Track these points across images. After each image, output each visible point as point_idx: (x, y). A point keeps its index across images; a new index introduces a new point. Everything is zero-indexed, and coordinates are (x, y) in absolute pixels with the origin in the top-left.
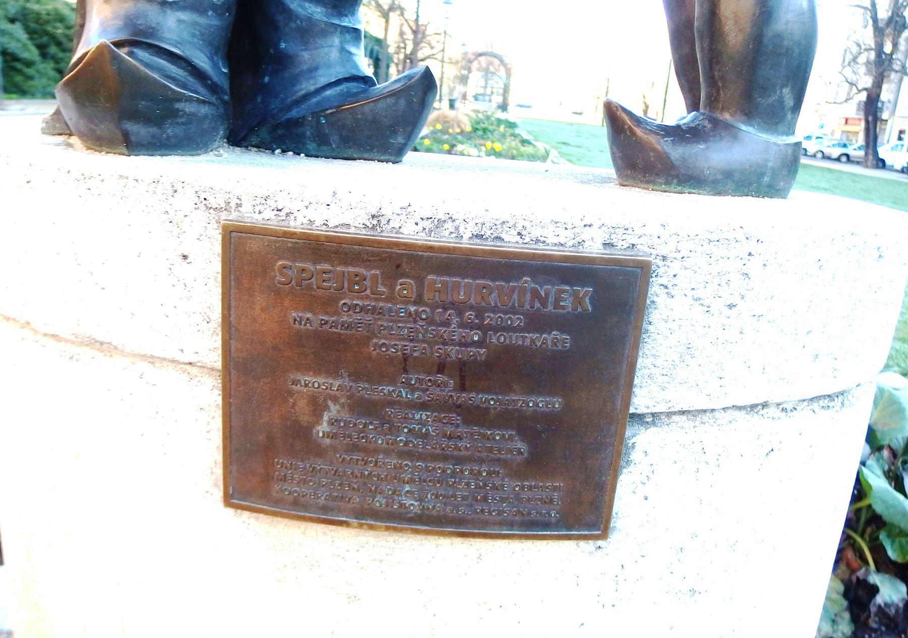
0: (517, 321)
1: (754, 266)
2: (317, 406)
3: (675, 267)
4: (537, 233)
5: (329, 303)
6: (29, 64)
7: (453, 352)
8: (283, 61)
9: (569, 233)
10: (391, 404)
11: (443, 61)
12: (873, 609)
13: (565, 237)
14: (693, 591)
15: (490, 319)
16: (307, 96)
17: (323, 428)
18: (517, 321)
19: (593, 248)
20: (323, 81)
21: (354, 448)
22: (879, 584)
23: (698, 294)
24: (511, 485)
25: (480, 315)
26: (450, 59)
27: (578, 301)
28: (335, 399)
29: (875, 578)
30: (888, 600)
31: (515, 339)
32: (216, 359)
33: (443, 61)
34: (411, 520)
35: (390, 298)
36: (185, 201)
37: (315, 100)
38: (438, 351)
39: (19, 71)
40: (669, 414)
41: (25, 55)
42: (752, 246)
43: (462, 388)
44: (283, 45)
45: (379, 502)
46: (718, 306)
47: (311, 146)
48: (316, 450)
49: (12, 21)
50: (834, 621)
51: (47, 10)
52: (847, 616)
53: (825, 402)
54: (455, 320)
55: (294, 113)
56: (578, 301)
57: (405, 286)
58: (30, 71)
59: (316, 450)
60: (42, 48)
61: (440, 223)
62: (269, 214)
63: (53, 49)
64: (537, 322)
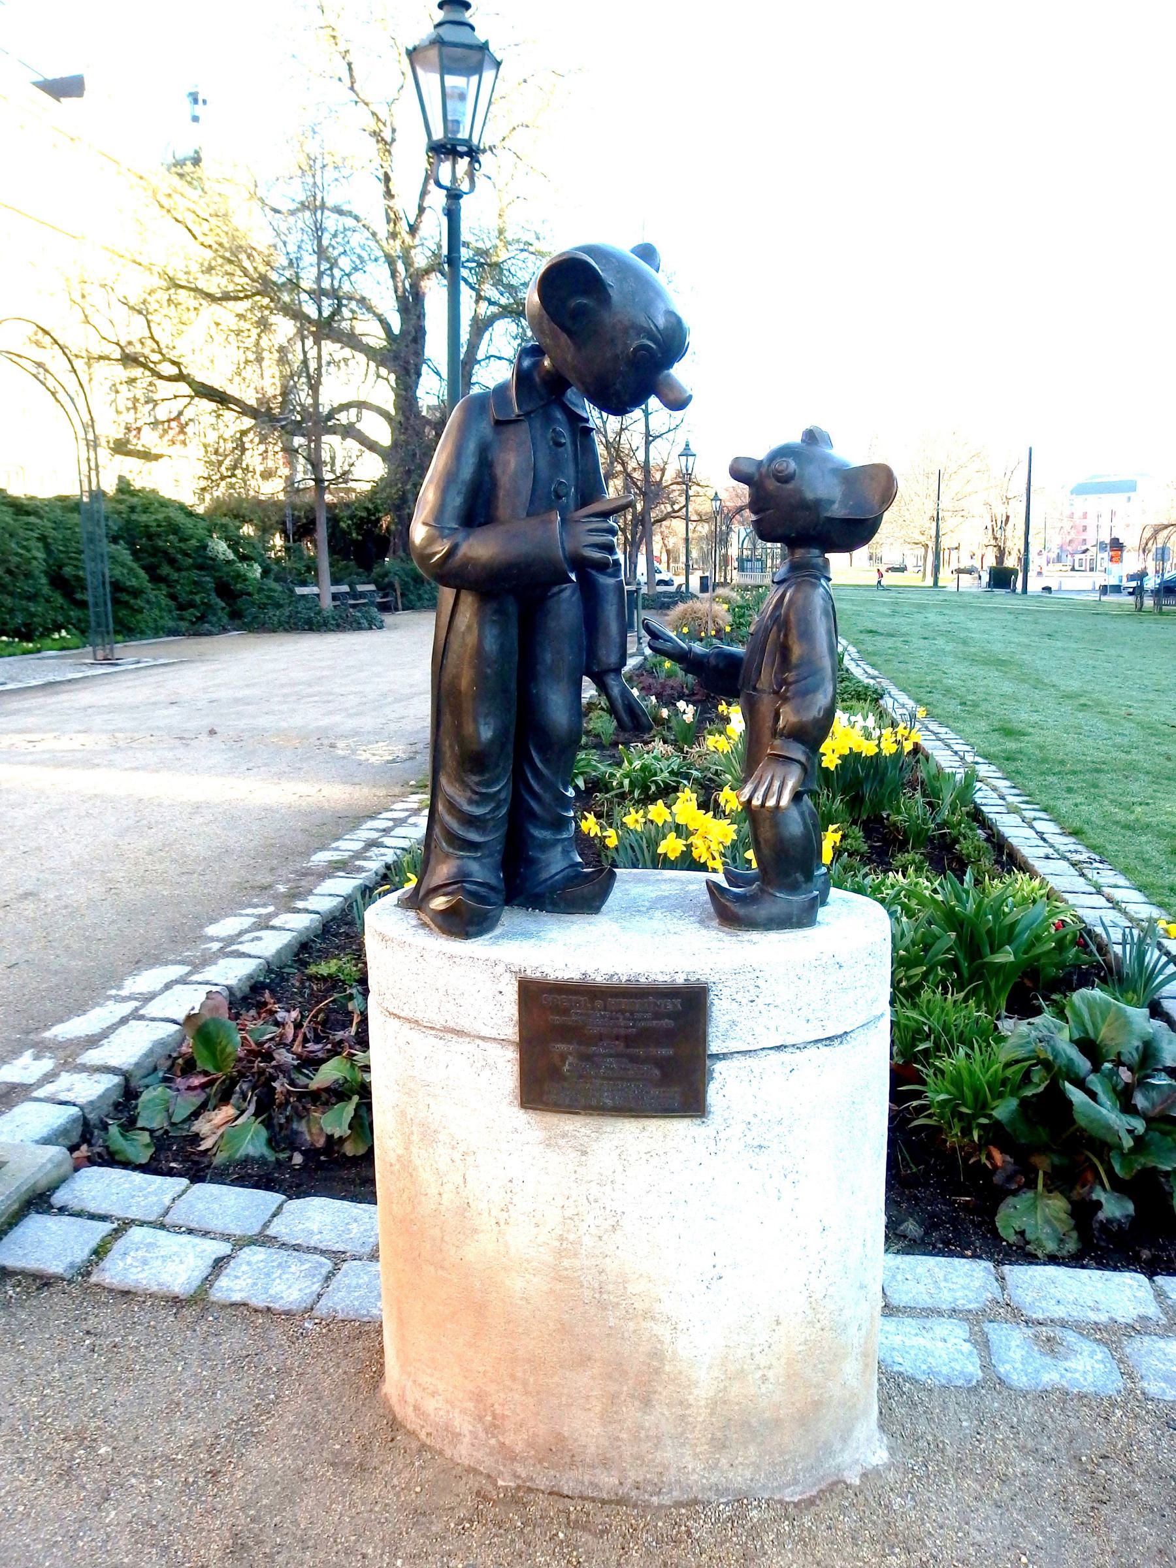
0: (649, 1015)
1: (760, 982)
2: (563, 1057)
3: (720, 986)
4: (653, 977)
5: (565, 1012)
6: (136, 593)
7: (622, 1031)
8: (531, 862)
10: (597, 1055)
11: (687, 519)
12: (1096, 1225)
13: (667, 978)
14: (761, 1147)
15: (639, 1016)
16: (546, 880)
17: (566, 1068)
18: (649, 1015)
19: (680, 980)
20: (553, 872)
21: (581, 1077)
22: (1103, 1201)
24: (655, 1092)
25: (632, 1014)
26: (699, 514)
27: (675, 1005)
28: (570, 1054)
29: (1099, 1195)
30: (1110, 1215)
31: (649, 1024)
32: (511, 1032)
33: (687, 519)
34: (609, 1110)
35: (593, 1009)
36: (500, 969)
37: (549, 882)
38: (615, 1031)
39: (126, 604)
40: (732, 1053)
41: (134, 582)
42: (757, 973)
43: (627, 1046)
45: (594, 1103)
46: (744, 1001)
47: (549, 908)
48: (563, 1078)
49: (115, 540)
50: (1061, 1240)
51: (156, 520)
52: (1074, 1235)
53: (828, 1042)
54: (621, 1017)
55: (538, 890)
56: (675, 1005)
57: (599, 1003)
58: (140, 603)
59: (563, 1078)
60: (151, 570)
61: (612, 976)
62: (538, 974)
63: (165, 570)
64: (657, 1016)
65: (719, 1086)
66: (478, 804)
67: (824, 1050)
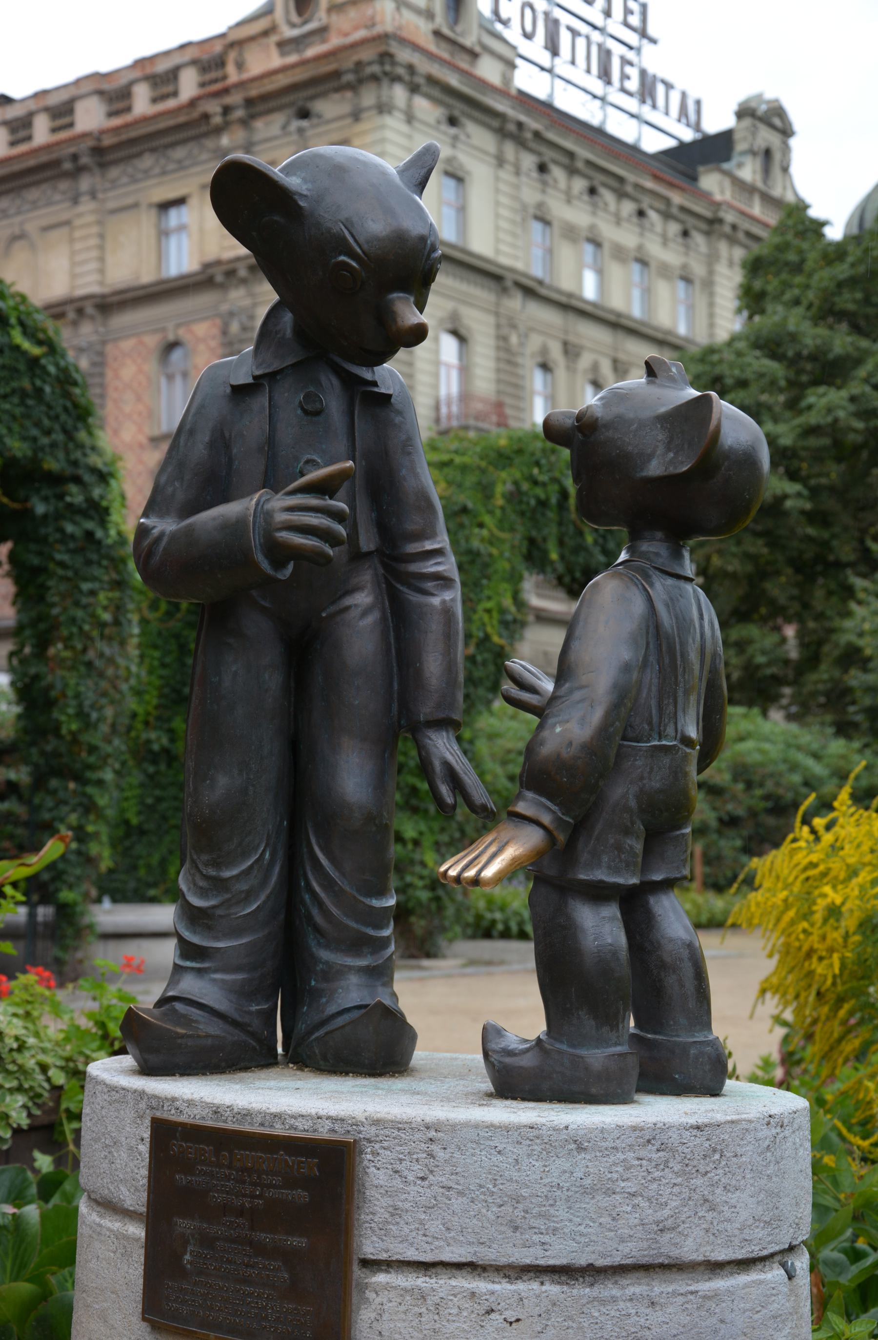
1: (435, 1148)
9: (310, 1123)
23: (398, 1167)
42: (432, 1134)
44: (313, 983)
46: (411, 1178)
65: (373, 1315)
66: (203, 893)
67: (552, 1289)
